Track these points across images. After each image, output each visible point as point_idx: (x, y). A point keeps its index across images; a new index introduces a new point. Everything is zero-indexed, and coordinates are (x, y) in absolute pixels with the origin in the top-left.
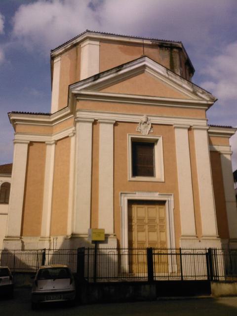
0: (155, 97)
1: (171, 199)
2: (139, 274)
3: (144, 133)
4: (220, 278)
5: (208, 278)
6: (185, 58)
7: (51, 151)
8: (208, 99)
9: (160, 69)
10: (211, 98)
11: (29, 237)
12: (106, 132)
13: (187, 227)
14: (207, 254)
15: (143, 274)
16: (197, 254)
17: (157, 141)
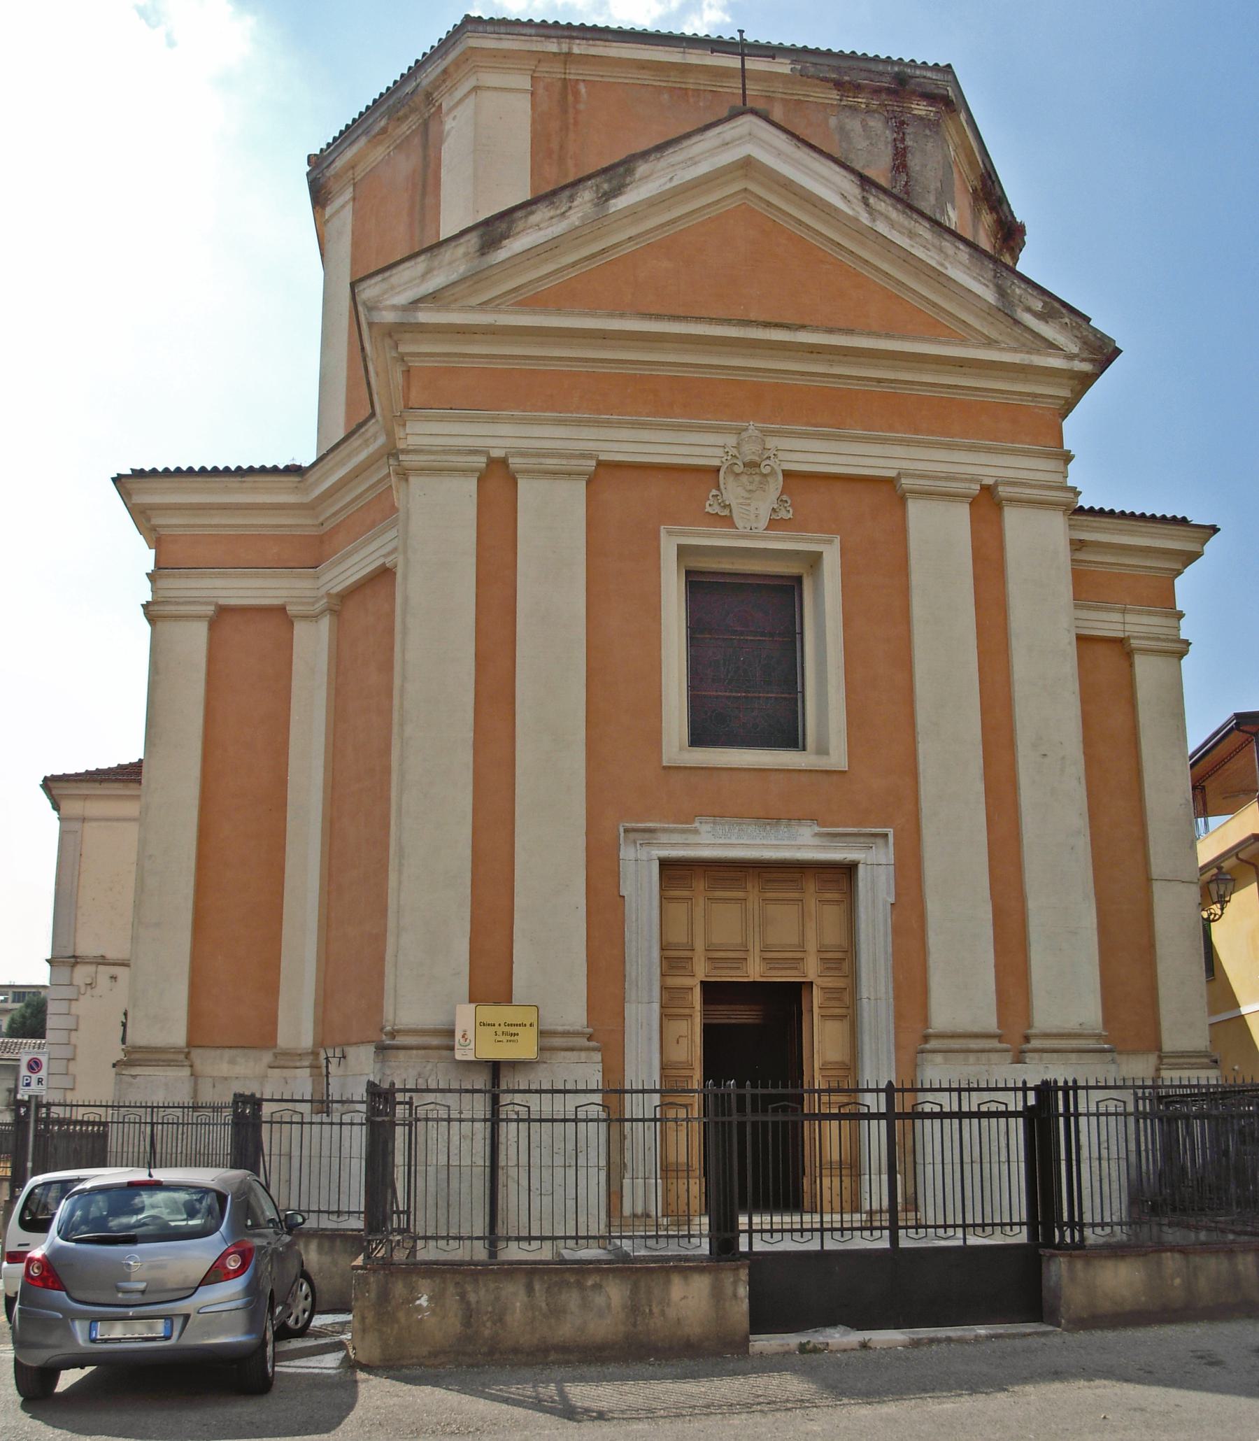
0: (803, 327)
1: (877, 867)
2: (847, 1217)
3: (750, 528)
4: (1088, 1232)
5: (1033, 1234)
6: (972, 163)
7: (312, 646)
8: (1074, 349)
9: (827, 182)
10: (1085, 343)
11: (228, 1053)
12: (553, 521)
13: (962, 994)
14: (1028, 1114)
15: (837, 1217)
16: (979, 1115)
17: (814, 560)
